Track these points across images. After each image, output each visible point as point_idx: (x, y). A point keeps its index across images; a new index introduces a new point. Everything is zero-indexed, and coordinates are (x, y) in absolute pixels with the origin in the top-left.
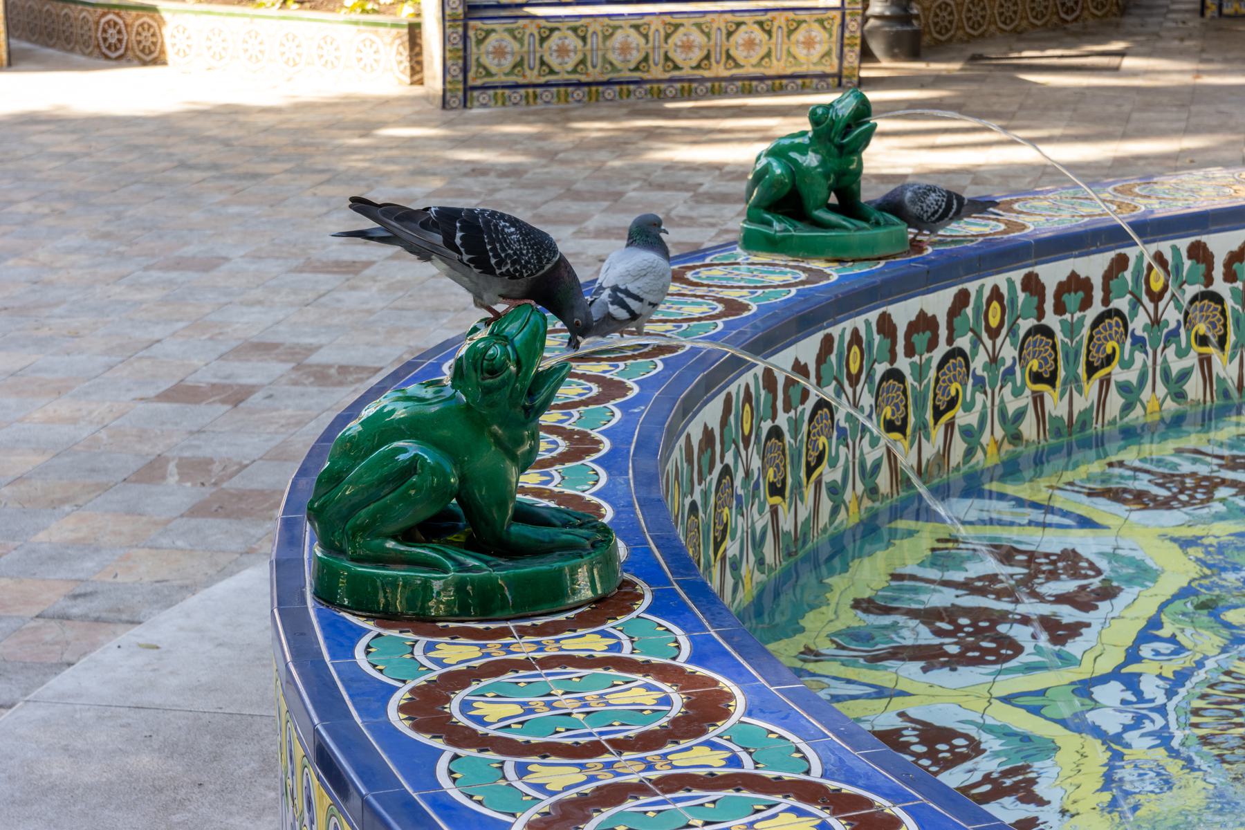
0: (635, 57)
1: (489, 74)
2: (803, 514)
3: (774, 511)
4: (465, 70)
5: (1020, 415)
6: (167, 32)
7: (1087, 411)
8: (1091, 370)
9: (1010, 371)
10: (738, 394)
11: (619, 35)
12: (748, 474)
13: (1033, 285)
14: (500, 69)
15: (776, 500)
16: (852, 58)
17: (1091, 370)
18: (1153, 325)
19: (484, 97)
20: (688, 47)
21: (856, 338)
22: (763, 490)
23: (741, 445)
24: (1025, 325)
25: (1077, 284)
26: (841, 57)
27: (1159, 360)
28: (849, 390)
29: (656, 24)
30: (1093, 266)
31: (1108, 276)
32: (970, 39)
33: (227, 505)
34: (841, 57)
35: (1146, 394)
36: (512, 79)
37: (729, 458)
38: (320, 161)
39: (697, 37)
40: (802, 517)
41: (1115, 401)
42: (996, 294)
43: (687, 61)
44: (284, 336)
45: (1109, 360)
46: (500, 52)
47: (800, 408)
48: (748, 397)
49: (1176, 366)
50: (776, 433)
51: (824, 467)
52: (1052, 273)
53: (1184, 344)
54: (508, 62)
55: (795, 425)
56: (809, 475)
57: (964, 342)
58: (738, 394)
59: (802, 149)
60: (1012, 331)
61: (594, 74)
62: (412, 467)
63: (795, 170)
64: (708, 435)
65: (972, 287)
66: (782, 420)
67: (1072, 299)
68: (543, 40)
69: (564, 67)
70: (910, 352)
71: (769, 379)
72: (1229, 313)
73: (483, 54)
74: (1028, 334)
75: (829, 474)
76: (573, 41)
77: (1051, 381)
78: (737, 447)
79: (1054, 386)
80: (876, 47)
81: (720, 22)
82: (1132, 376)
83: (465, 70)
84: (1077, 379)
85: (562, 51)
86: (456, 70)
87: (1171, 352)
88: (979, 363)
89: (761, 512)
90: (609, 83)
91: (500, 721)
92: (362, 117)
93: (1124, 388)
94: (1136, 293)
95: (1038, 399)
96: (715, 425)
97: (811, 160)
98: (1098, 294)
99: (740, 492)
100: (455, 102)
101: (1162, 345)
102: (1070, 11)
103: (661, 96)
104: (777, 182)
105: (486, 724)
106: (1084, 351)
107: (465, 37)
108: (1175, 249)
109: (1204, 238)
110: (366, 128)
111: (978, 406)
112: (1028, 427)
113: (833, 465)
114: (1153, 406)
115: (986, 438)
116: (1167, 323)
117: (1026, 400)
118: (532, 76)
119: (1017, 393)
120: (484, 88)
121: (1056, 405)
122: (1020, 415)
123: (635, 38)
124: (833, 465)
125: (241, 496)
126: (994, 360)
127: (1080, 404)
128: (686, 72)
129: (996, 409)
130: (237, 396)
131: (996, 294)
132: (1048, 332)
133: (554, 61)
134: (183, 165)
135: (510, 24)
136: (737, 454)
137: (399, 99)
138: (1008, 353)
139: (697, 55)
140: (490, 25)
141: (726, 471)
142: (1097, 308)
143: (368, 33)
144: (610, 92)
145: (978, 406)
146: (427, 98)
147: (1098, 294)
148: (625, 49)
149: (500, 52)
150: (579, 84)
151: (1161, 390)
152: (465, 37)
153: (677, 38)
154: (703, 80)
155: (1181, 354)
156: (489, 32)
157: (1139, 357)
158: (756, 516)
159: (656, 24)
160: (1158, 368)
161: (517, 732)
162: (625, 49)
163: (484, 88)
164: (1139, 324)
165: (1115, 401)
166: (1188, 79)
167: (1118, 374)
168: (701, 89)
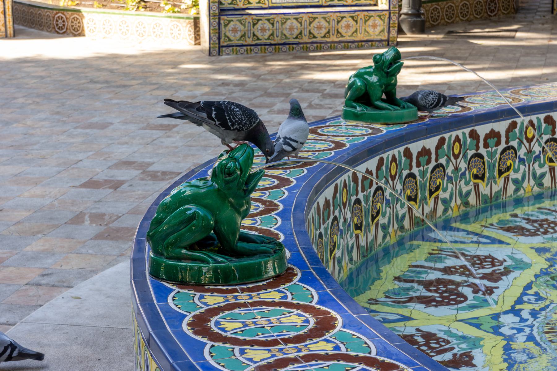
0: (296, 32)
1: (230, 40)
2: (370, 238)
3: (357, 237)
4: (219, 39)
5: (468, 193)
6: (85, 21)
8: (500, 173)
9: (464, 174)
11: (289, 23)
12: (345, 220)
13: (474, 135)
14: (235, 38)
15: (358, 232)
16: (394, 33)
17: (500, 173)
18: (528, 153)
19: (228, 50)
20: (319, 28)
21: (394, 159)
22: (352, 227)
24: (470, 153)
25: (494, 135)
26: (389, 32)
27: (531, 169)
28: (391, 182)
29: (305, 17)
30: (501, 127)
32: (447, 24)
33: (111, 234)
34: (389, 32)
35: (525, 184)
36: (240, 42)
38: (154, 80)
39: (324, 23)
41: (511, 187)
42: (457, 139)
43: (319, 34)
44: (138, 158)
45: (508, 169)
46: (235, 30)
47: (369, 190)
48: (345, 186)
51: (380, 217)
52: (483, 130)
53: (542, 162)
54: (238, 35)
55: (367, 198)
56: (373, 221)
57: (443, 161)
58: (341, 184)
59: (370, 74)
60: (465, 156)
61: (277, 40)
62: (193, 217)
63: (367, 83)
64: (327, 202)
65: (447, 136)
66: (361, 196)
67: (492, 141)
68: (254, 25)
69: (264, 37)
72: (486, 163)
73: (228, 31)
76: (268, 25)
77: (482, 178)
78: (340, 208)
79: (483, 181)
80: (405, 27)
81: (334, 16)
82: (519, 176)
83: (219, 39)
84: (494, 177)
85: (263, 30)
86: (215, 38)
87: (536, 165)
88: (449, 170)
89: (351, 237)
90: (284, 44)
91: (232, 330)
92: (173, 59)
93: (515, 181)
94: (520, 138)
95: (476, 186)
97: (374, 79)
98: (503, 139)
99: (342, 228)
100: (215, 53)
101: (532, 162)
102: (492, 11)
103: (308, 50)
104: (358, 89)
105: (226, 332)
106: (497, 165)
107: (219, 24)
108: (538, 119)
110: (175, 65)
112: (472, 199)
113: (384, 216)
114: (528, 189)
115: (453, 204)
116: (535, 152)
117: (471, 187)
118: (249, 41)
119: (467, 184)
120: (228, 46)
121: (484, 189)
122: (468, 193)
123: (296, 24)
124: (384, 216)
125: (118, 230)
126: (457, 169)
127: (495, 189)
128: (319, 39)
130: (116, 185)
131: (457, 139)
132: (481, 156)
133: (259, 34)
134: (92, 81)
135: (239, 18)
136: (340, 211)
137: (190, 51)
138: (463, 166)
139: (324, 31)
140: (230, 18)
141: (335, 219)
142: (503, 145)
143: (176, 22)
144: (284, 48)
146: (202, 51)
147: (503, 139)
148: (291, 29)
149: (235, 30)
150: (271, 45)
151: (532, 182)
152: (219, 24)
153: (315, 24)
154: (326, 43)
155: (541, 166)
156: (230, 21)
157: (522, 167)
158: (349, 239)
159: (305, 17)
160: (531, 173)
162: (291, 29)
163: (228, 46)
164: (522, 152)
165: (511, 187)
166: (546, 42)
167: (512, 175)
168: (326, 47)
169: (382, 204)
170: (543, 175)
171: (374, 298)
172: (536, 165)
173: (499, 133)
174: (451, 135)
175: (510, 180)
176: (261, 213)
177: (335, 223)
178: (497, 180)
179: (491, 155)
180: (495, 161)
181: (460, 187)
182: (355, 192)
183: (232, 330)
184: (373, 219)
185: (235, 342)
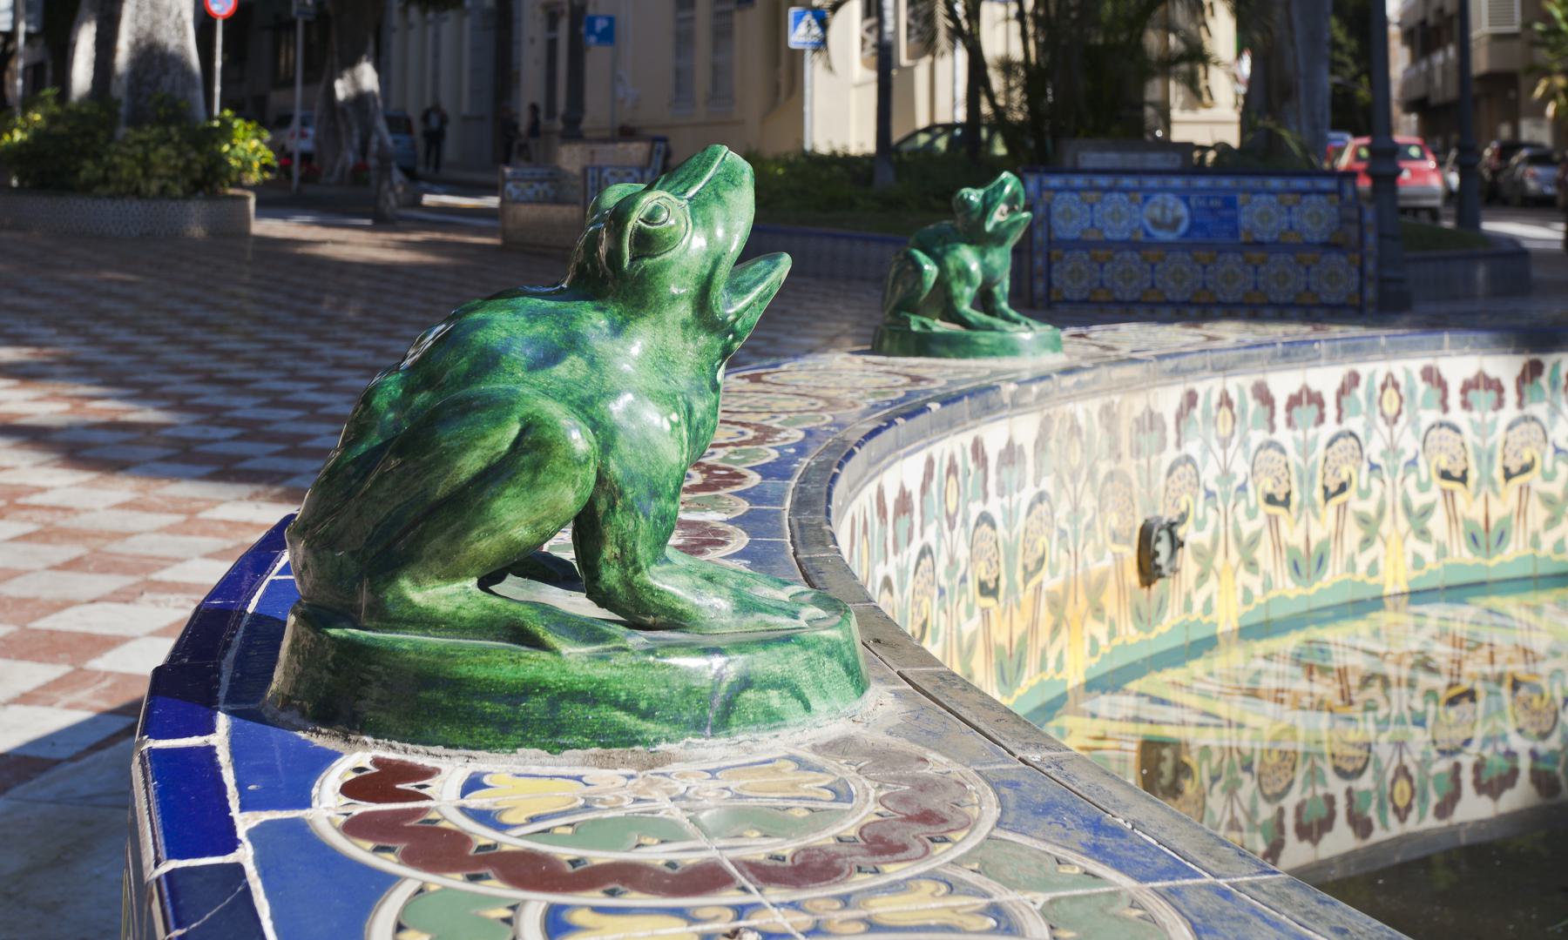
2: (1019, 628)
3: (986, 612)
7: (1324, 545)
10: (941, 459)
12: (952, 561)
15: (989, 602)
22: (972, 586)
23: (945, 525)
28: (1070, 487)
31: (1342, 392)
37: (931, 530)
40: (1018, 631)
47: (1016, 496)
48: (952, 469)
49: (1418, 500)
50: (985, 518)
51: (1044, 574)
55: (1010, 515)
56: (1026, 582)
58: (941, 459)
70: (1137, 451)
71: (978, 450)
74: (1261, 447)
75: (1050, 582)
78: (940, 525)
82: (1370, 507)
84: (1313, 505)
89: (970, 615)
91: (532, 820)
96: (914, 488)
99: (943, 582)
105: (502, 827)
106: (1319, 474)
109: (1142, 635)
111: (1210, 526)
113: (1054, 575)
116: (1403, 452)
117: (1260, 522)
119: (1251, 514)
121: (1292, 535)
124: (1054, 575)
129: (1230, 529)
136: (940, 535)
141: (925, 552)
145: (1210, 526)
158: (963, 619)
161: (562, 841)
165: (1353, 534)
169: (1049, 538)
170: (1427, 511)
171: (1130, 553)
172: (1411, 480)
173: (1319, 395)
174: (1210, 389)
175: (1349, 513)
176: (704, 487)
177: (926, 562)
178: (1320, 510)
179: (1305, 449)
180: (1315, 463)
181: (1236, 522)
182: (981, 493)
183: (532, 820)
184: (1028, 575)
185: (528, 871)
